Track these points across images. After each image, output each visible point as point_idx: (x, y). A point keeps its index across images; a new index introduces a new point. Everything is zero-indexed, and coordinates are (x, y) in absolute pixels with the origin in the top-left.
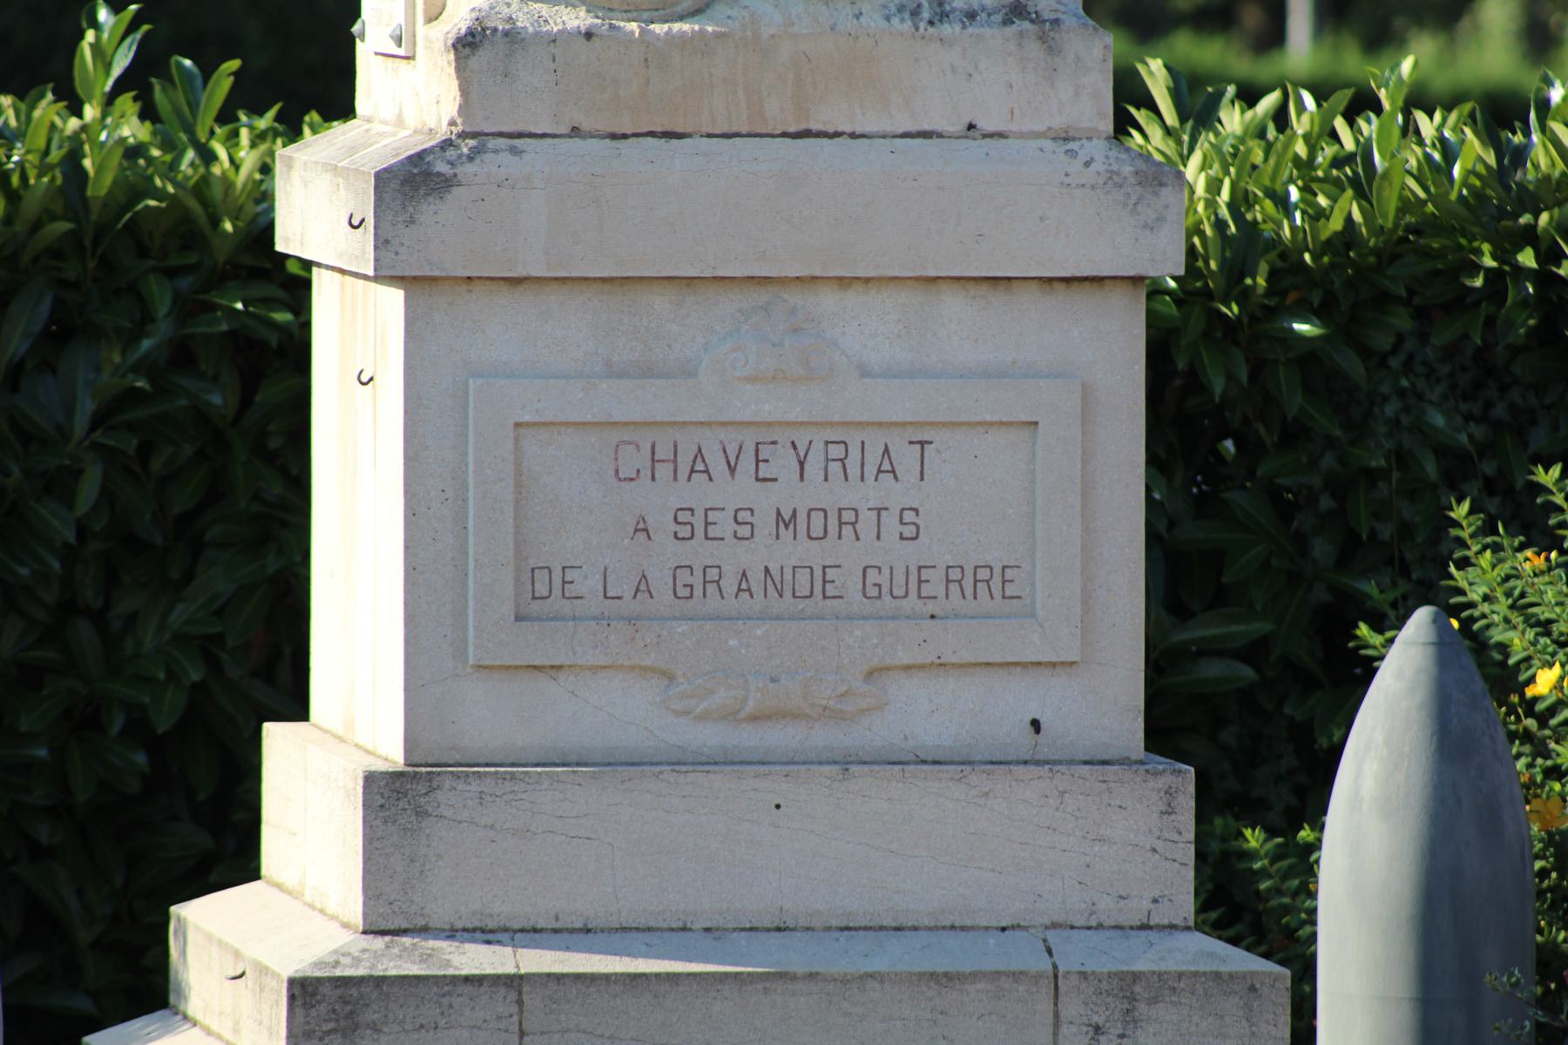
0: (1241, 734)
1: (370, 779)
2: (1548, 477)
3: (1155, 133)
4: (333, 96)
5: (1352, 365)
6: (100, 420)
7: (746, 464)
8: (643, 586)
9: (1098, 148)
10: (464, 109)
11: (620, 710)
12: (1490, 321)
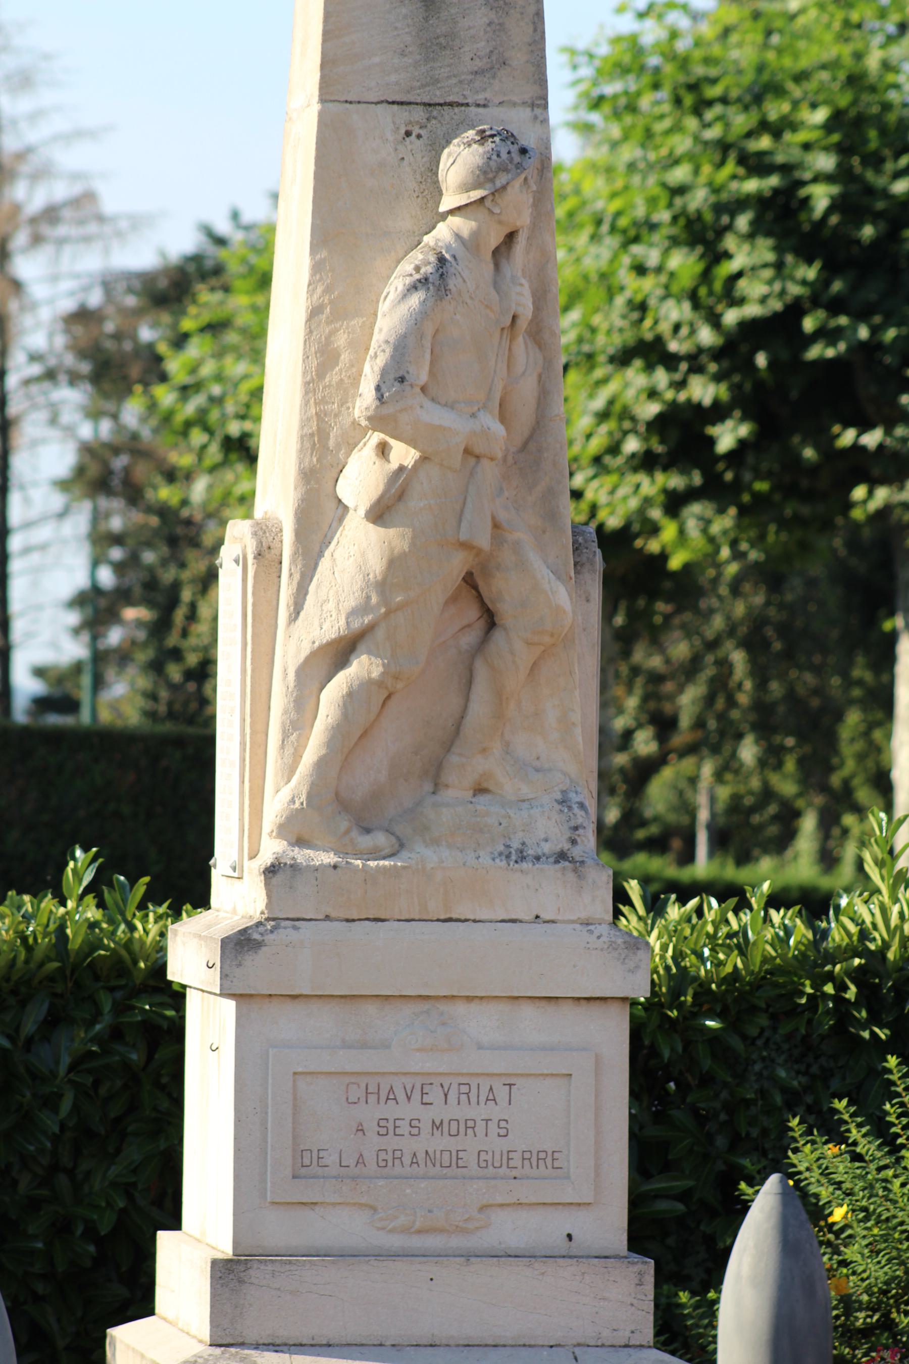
0: (678, 1240)
1: (215, 1263)
2: (840, 1105)
3: (633, 919)
4: (202, 901)
5: (736, 1043)
6: (72, 1068)
7: (417, 1096)
8: (360, 1160)
9: (604, 929)
10: (268, 906)
11: (347, 1227)
12: (810, 1022)
